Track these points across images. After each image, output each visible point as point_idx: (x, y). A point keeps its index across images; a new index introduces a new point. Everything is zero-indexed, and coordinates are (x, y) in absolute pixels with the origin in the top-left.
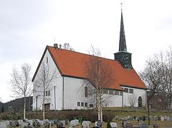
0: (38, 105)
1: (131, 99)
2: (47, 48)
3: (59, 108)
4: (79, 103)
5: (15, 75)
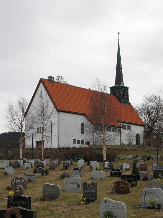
0: (30, 143)
1: (128, 135)
2: (42, 81)
3: (55, 146)
4: (75, 140)
5: (11, 108)
